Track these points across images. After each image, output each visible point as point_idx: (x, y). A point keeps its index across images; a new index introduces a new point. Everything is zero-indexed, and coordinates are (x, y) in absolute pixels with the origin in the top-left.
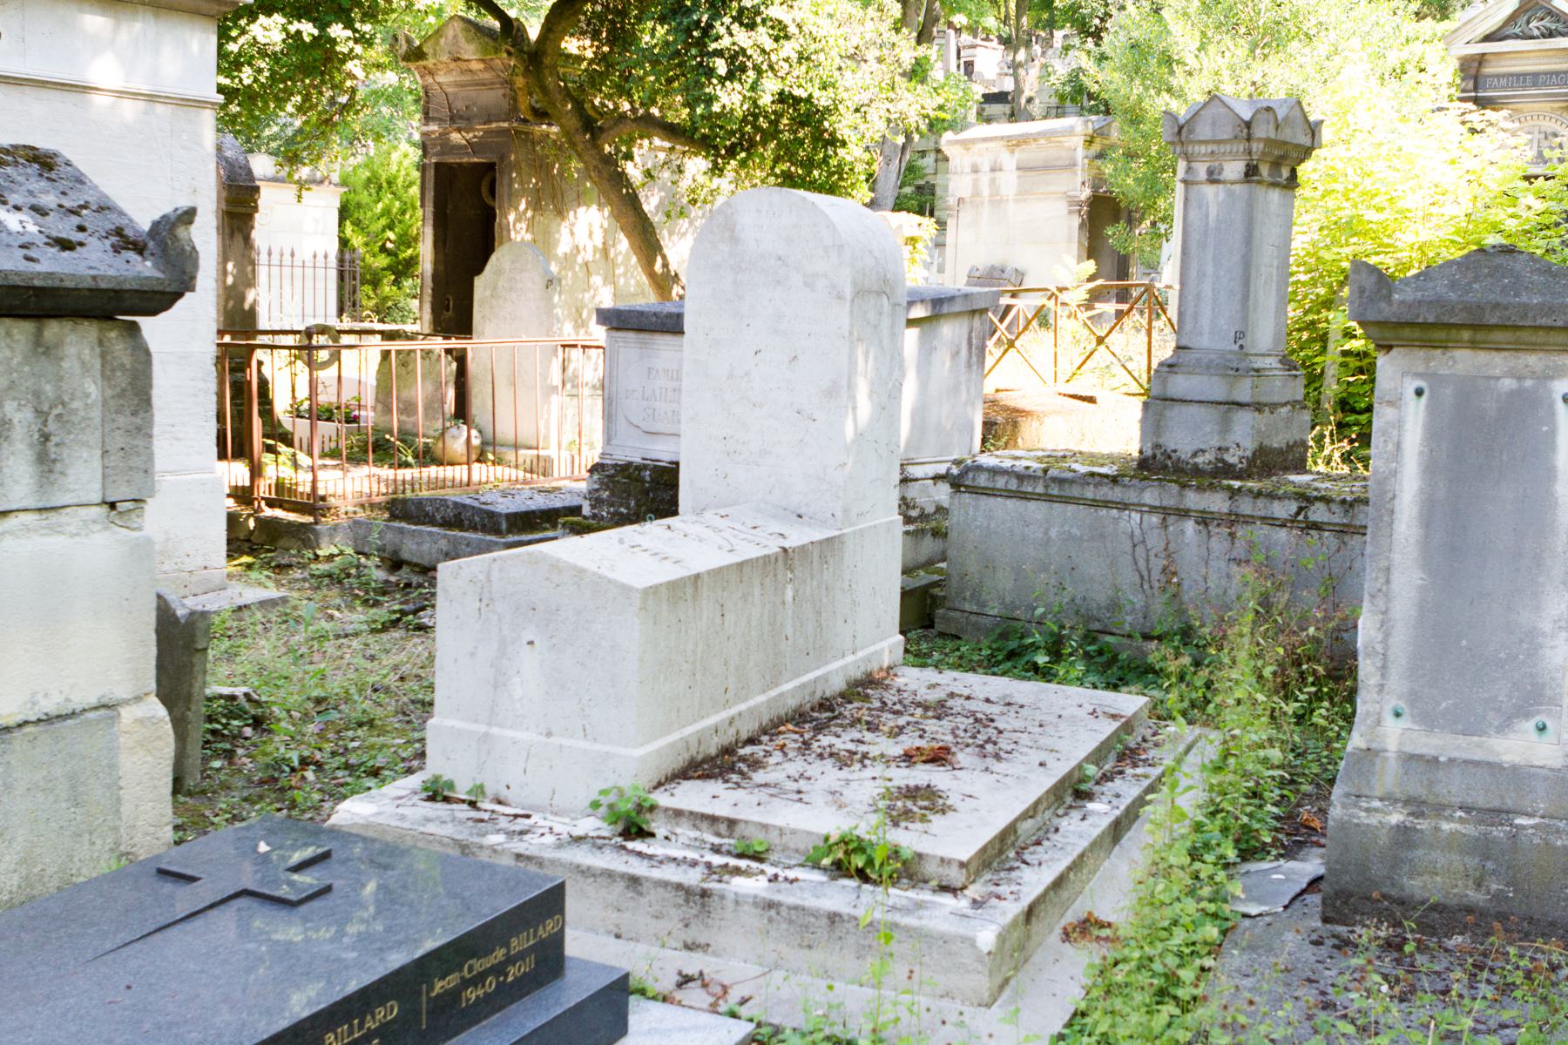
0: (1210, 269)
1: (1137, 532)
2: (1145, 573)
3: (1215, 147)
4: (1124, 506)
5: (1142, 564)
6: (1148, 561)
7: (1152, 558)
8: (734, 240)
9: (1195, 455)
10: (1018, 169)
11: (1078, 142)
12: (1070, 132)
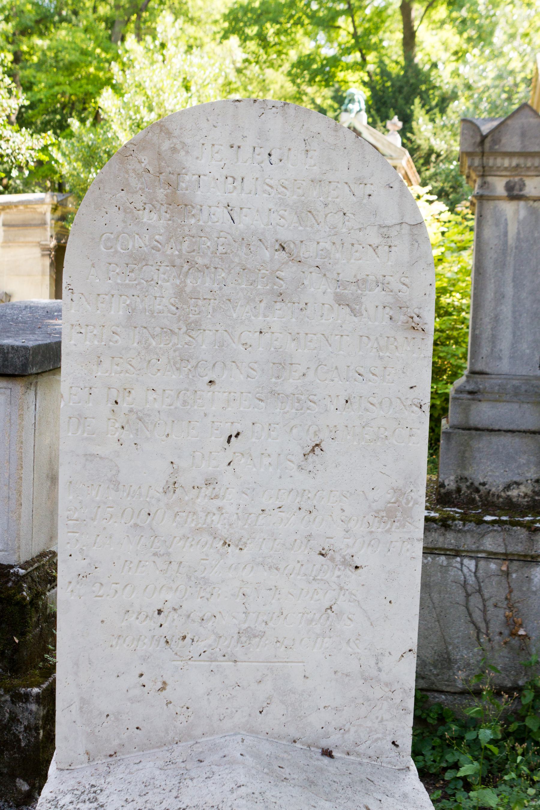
0: (509, 291)
1: (472, 580)
2: (482, 626)
3: (521, 161)
4: (457, 553)
5: (477, 615)
6: (484, 611)
7: (491, 609)
8: (178, 204)
9: (508, 487)
10: (4, 225)
11: (47, 209)
12: (42, 202)
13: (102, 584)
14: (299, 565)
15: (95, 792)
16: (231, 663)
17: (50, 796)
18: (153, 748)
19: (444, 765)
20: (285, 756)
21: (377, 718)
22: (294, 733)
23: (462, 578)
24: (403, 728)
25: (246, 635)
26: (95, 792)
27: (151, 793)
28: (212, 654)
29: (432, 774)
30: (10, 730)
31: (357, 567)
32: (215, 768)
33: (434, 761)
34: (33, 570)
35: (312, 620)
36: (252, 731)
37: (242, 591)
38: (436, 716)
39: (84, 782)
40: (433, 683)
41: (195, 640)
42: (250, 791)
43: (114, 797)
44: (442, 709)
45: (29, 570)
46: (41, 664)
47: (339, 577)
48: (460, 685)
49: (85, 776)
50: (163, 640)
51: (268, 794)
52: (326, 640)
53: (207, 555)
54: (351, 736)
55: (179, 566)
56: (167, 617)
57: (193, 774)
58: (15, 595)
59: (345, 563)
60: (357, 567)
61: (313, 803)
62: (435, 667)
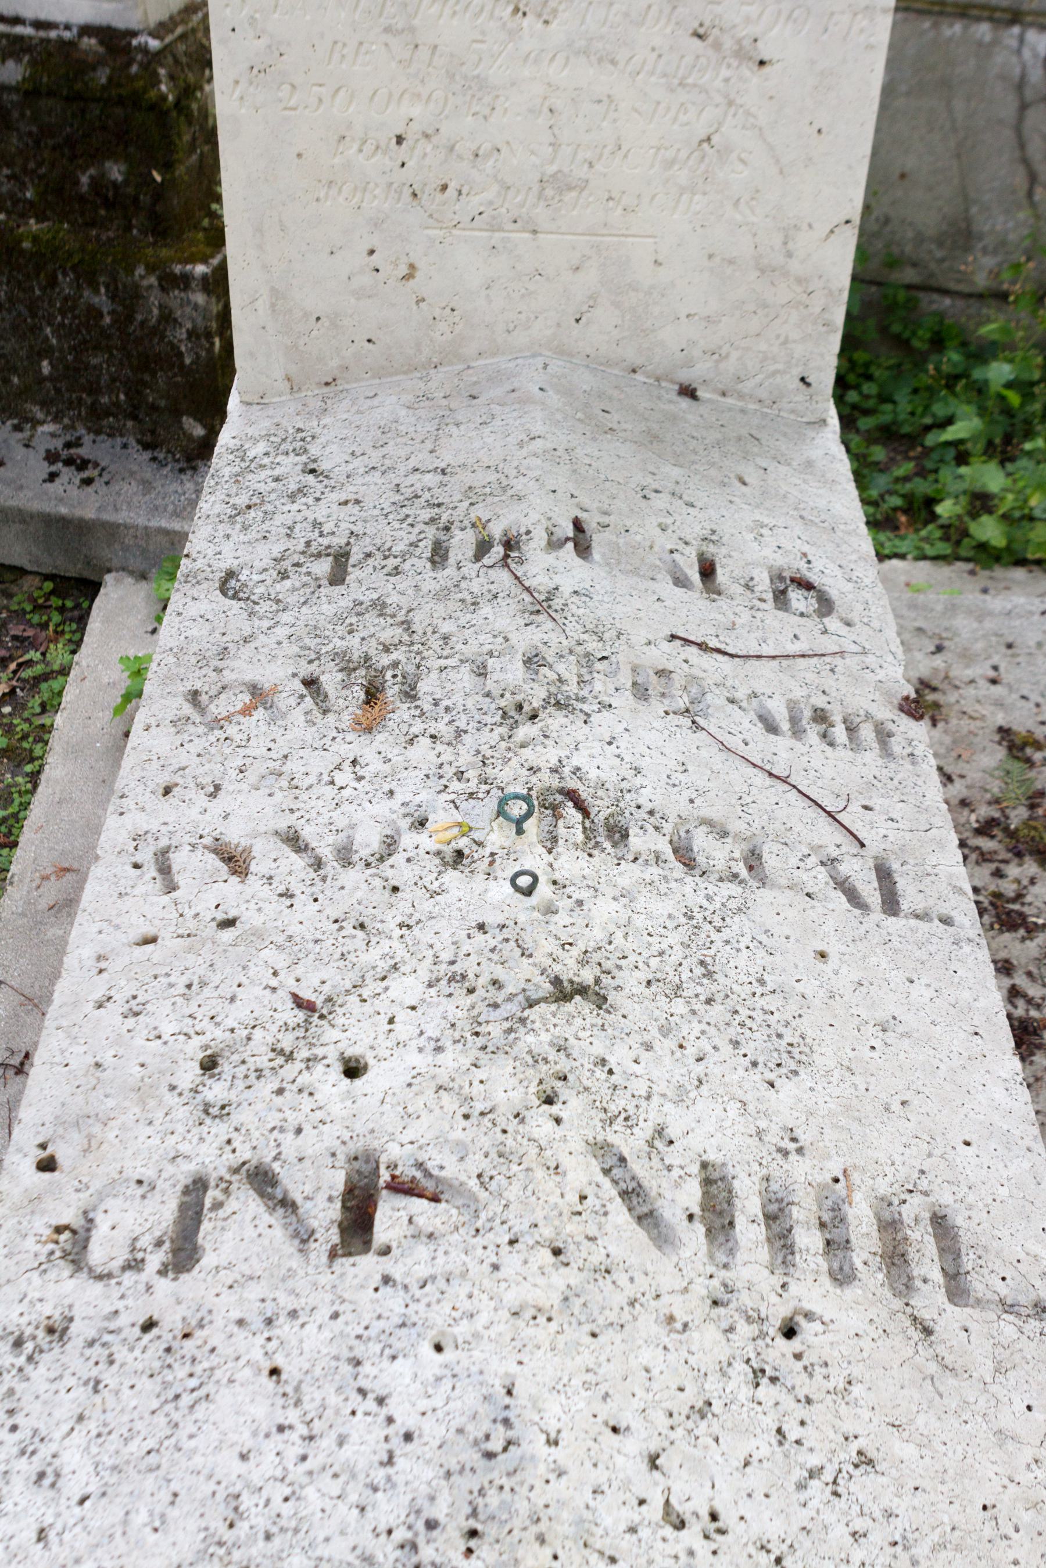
13: (293, 86)
14: (655, 55)
15: (303, 440)
16: (527, 235)
17: (232, 444)
18: (397, 374)
19: (928, 421)
20: (616, 393)
21: (778, 337)
22: (632, 357)
23: (1017, 71)
24: (822, 355)
25: (556, 186)
26: (303, 440)
27: (391, 443)
28: (494, 218)
29: (904, 436)
30: (163, 337)
31: (762, 63)
32: (496, 409)
33: (912, 414)
34: (176, 40)
35: (673, 162)
36: (563, 352)
37: (547, 104)
38: (928, 336)
39: (284, 423)
40: (932, 275)
41: (464, 191)
42: (550, 446)
43: (333, 448)
44: (941, 323)
45: (169, 39)
46: (206, 222)
47: (727, 80)
48: (981, 281)
49: (287, 415)
50: (407, 192)
51: (579, 452)
52: (697, 198)
53: (483, 33)
54: (731, 366)
55: (433, 54)
56: (413, 149)
57: (460, 418)
58: (145, 91)
59: (740, 54)
60: (762, 63)
61: (652, 469)
62: (941, 244)
